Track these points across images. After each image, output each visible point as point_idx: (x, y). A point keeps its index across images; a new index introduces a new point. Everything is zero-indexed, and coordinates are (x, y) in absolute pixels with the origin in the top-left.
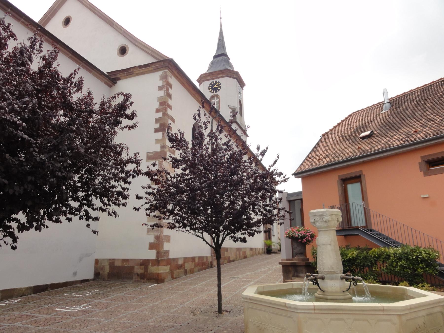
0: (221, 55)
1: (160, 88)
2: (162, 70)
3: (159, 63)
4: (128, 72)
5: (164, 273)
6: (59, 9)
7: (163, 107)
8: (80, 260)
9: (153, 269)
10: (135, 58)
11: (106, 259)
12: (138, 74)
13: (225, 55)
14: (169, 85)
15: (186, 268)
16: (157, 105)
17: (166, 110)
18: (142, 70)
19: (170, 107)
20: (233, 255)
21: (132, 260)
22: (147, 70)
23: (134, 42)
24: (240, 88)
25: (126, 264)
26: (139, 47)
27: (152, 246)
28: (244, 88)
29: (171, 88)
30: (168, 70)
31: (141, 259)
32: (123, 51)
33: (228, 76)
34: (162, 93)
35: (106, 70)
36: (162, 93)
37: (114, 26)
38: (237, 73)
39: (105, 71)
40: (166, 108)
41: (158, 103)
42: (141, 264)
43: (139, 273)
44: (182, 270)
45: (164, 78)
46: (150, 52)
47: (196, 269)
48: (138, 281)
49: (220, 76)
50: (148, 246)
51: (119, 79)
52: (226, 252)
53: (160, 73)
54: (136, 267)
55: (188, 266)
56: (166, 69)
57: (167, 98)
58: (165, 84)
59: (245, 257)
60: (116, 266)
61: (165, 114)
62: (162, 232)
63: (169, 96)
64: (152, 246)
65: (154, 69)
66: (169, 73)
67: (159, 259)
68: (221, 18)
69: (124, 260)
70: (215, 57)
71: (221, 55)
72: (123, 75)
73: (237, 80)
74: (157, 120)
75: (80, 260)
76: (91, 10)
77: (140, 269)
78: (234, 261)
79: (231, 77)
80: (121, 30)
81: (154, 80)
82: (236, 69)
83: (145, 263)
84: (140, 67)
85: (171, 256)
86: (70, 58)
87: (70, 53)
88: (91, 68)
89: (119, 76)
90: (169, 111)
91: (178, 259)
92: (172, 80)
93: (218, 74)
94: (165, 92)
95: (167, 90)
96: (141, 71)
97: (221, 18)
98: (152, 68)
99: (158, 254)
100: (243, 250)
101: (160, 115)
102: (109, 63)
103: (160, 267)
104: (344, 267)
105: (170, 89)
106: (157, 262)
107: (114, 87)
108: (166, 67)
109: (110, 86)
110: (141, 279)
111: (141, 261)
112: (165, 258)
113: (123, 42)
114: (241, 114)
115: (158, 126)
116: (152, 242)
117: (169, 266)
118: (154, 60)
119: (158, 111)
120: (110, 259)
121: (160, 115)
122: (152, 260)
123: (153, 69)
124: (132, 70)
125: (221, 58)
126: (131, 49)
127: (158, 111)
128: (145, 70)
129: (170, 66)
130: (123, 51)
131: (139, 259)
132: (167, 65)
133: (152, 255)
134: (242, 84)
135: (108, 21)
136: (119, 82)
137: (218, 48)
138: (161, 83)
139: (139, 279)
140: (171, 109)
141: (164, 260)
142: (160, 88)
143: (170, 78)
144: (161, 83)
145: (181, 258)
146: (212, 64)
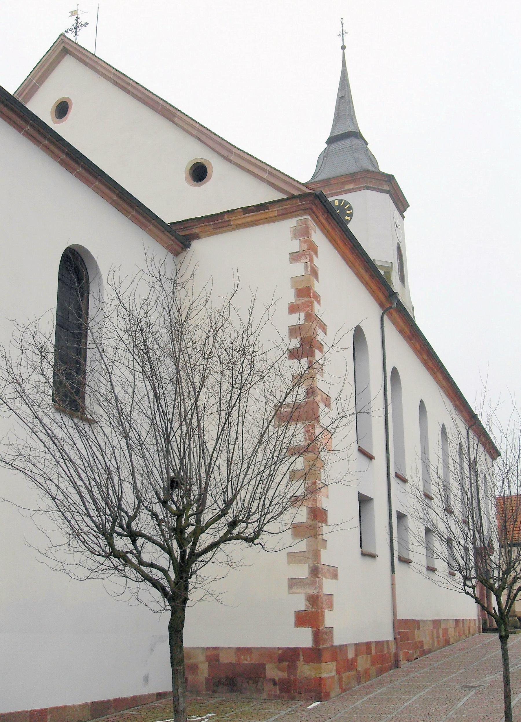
0: (345, 135)
1: (295, 257)
2: (296, 216)
3: (289, 202)
4: (218, 223)
5: (329, 678)
6: (41, 85)
7: (307, 299)
8: (152, 650)
9: (305, 670)
10: (228, 191)
11: (198, 648)
12: (239, 227)
13: (357, 135)
14: (313, 248)
15: (359, 669)
16: (290, 297)
17: (312, 308)
18: (250, 217)
19: (317, 298)
20: (428, 639)
21: (257, 649)
22: (263, 216)
23: (226, 154)
24: (397, 213)
25: (246, 660)
26: (236, 164)
27: (302, 619)
28: (405, 214)
29: (316, 254)
30: (310, 215)
31: (279, 649)
32: (199, 173)
33: (367, 188)
34: (299, 269)
35: (169, 217)
36: (299, 269)
37: (176, 120)
38: (390, 179)
39: (168, 220)
40: (312, 302)
41: (293, 291)
42: (281, 659)
43: (277, 679)
44: (353, 673)
45: (303, 233)
46: (265, 176)
47: (373, 671)
48: (279, 697)
49: (347, 187)
50: (292, 619)
51: (197, 237)
52: (416, 631)
53: (292, 222)
54: (268, 666)
55: (363, 663)
56: (305, 214)
57: (312, 278)
58: (305, 247)
59: (447, 643)
60: (224, 664)
61: (309, 317)
62: (321, 588)
63: (315, 273)
64: (302, 619)
65: (279, 215)
66: (311, 223)
67: (321, 647)
68: (343, 48)
69: (240, 651)
70: (330, 141)
71: (345, 135)
72: (207, 229)
73: (391, 196)
74: (294, 331)
75: (152, 650)
76: (116, 84)
77: (279, 669)
78: (430, 651)
79: (375, 189)
80: (194, 128)
81: (279, 237)
82: (385, 167)
83: (289, 656)
84: (246, 210)
85: (337, 642)
86: (114, 204)
87: (114, 192)
88: (147, 219)
89: (196, 230)
90: (318, 310)
91: (346, 646)
92: (318, 237)
93: (344, 183)
94: (306, 266)
95: (311, 260)
96: (249, 220)
97: (343, 48)
98: (273, 212)
99: (317, 636)
100: (443, 626)
101: (298, 318)
102: (176, 202)
103: (323, 665)
104: (80, 705)
105: (314, 257)
106: (314, 654)
107: (181, 256)
108: (305, 211)
109: (176, 254)
110: (281, 691)
111: (280, 652)
112: (327, 645)
113: (198, 153)
114: (402, 279)
115: (295, 343)
116: (302, 609)
117: (334, 663)
118: (278, 196)
119: (293, 309)
120: (208, 649)
121: (298, 318)
122: (304, 649)
123: (276, 214)
124: (226, 218)
125: (347, 142)
126: (217, 167)
127: (293, 309)
128: (258, 217)
129: (313, 207)
130: (199, 173)
131: (275, 648)
132: (308, 206)
133: (303, 638)
134: (401, 204)
135: (160, 108)
136: (196, 245)
137: (338, 118)
138: (296, 246)
139: (278, 692)
140: (319, 302)
141: (328, 648)
142: (295, 257)
143: (312, 232)
144: (296, 246)
145: (350, 645)
146: (324, 157)
